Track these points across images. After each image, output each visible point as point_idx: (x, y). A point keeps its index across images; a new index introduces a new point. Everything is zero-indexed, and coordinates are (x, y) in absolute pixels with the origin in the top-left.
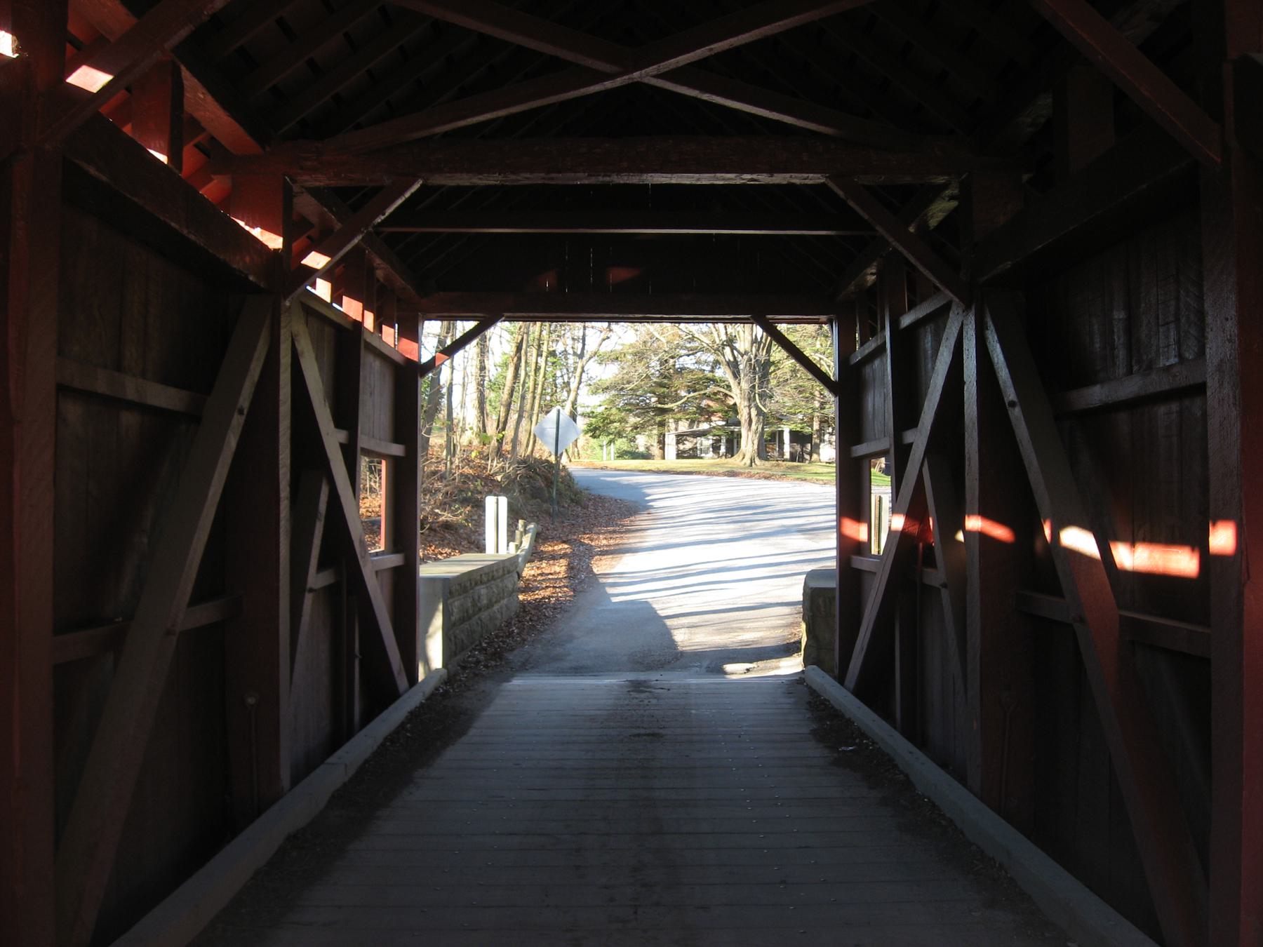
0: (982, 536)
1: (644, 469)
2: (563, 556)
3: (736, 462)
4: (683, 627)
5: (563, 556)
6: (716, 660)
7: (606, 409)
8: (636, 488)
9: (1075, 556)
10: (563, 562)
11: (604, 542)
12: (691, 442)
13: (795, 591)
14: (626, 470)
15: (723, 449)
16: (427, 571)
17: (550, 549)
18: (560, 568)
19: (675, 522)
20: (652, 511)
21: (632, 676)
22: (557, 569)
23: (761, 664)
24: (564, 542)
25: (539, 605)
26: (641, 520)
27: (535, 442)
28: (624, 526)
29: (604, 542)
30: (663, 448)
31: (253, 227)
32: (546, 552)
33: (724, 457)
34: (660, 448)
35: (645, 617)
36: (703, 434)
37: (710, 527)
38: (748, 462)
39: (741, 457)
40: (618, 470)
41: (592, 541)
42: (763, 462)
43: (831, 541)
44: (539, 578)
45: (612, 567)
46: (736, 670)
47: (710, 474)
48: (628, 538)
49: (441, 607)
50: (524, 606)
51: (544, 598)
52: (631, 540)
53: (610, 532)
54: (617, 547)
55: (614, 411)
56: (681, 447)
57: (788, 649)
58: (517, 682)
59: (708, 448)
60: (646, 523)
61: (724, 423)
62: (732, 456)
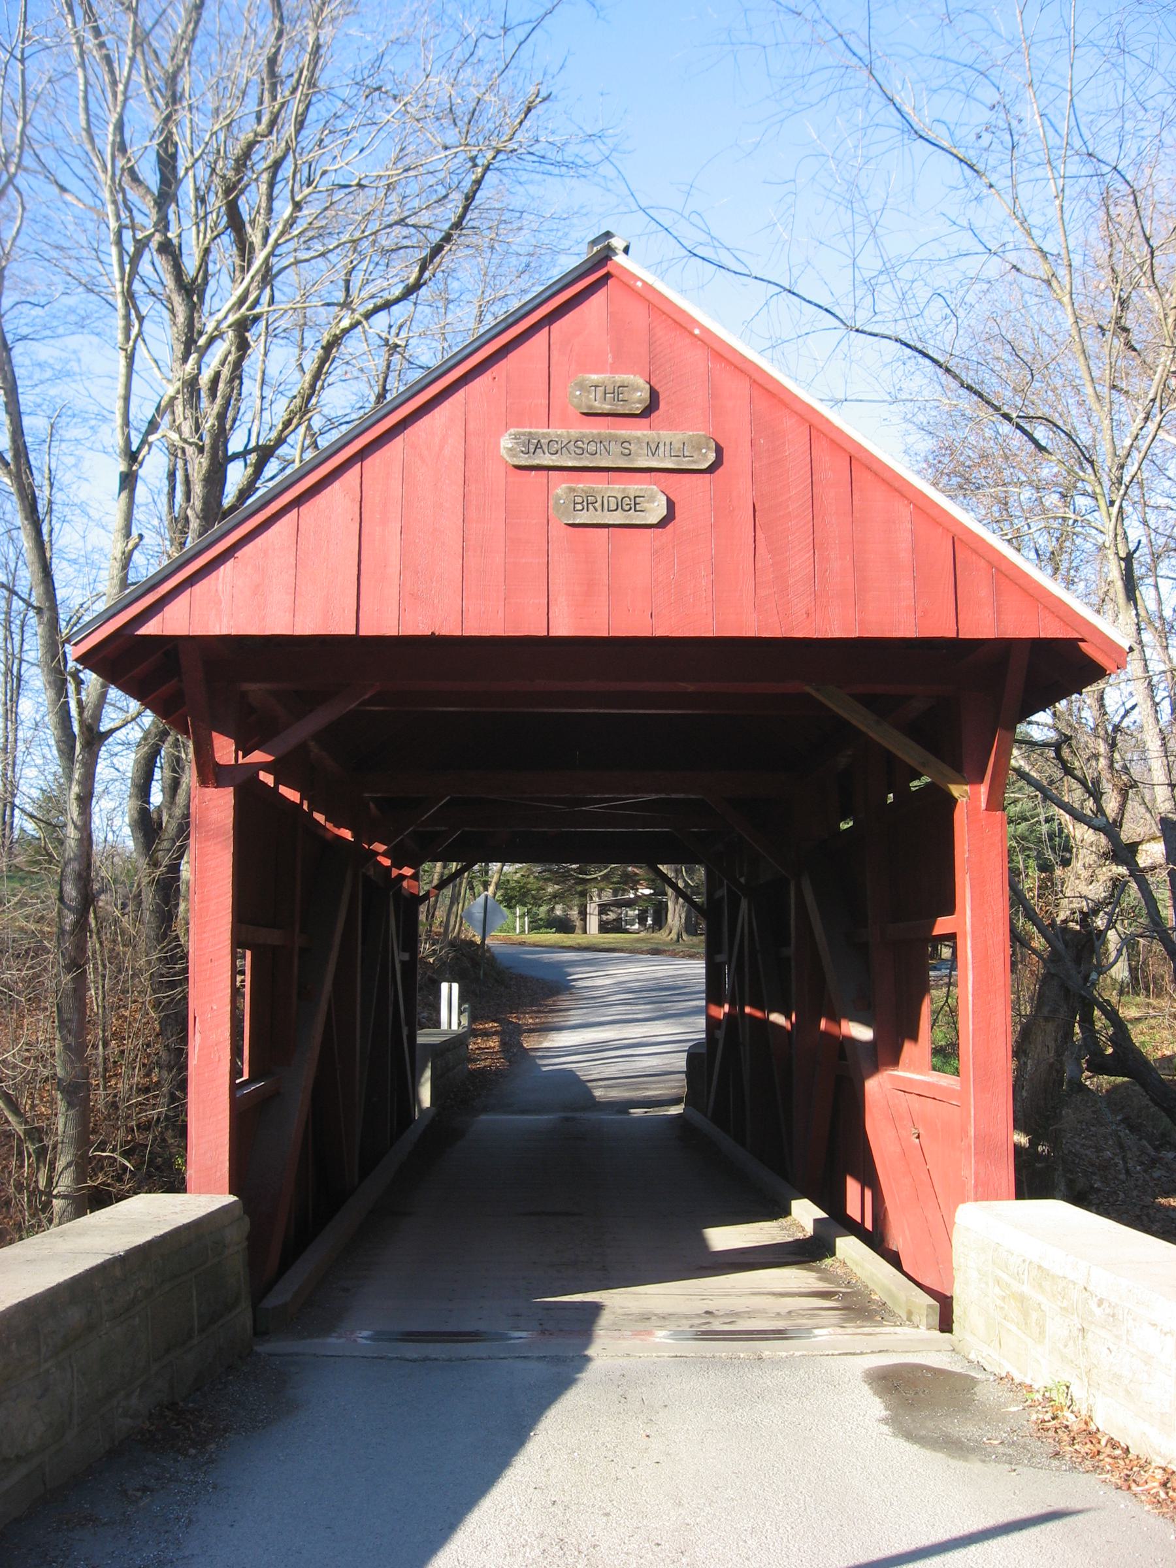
0: (750, 1015)
1: (564, 944)
2: (495, 1033)
3: (662, 936)
4: (601, 1087)
5: (495, 1033)
6: (624, 1106)
7: (523, 876)
8: (559, 965)
9: (775, 1025)
10: (496, 1038)
11: (531, 1021)
12: (615, 912)
13: (680, 1062)
14: (546, 946)
15: (650, 922)
16: (421, 1039)
17: (481, 1027)
18: (494, 1043)
19: (597, 1001)
20: (574, 991)
21: (563, 1115)
22: (492, 1045)
23: (656, 1109)
24: (494, 1021)
25: (482, 1071)
26: (564, 1001)
27: (461, 925)
28: (547, 1006)
29: (531, 1021)
30: (584, 920)
31: (339, 828)
32: (478, 1030)
33: (651, 930)
34: (581, 920)
35: (570, 1079)
36: (629, 904)
37: (628, 1007)
38: (675, 937)
39: (668, 932)
40: (538, 946)
41: (519, 1019)
42: (691, 938)
43: (701, 1022)
44: (477, 1052)
45: (541, 1043)
46: (638, 1112)
47: (633, 951)
48: (553, 1017)
49: (430, 1064)
50: (473, 1073)
51: (485, 1067)
52: (555, 1019)
53: (535, 1012)
54: (543, 1026)
55: (531, 879)
56: (604, 917)
57: (675, 1101)
58: (483, 1117)
59: (634, 920)
60: (567, 1003)
61: (652, 891)
62: (660, 930)
